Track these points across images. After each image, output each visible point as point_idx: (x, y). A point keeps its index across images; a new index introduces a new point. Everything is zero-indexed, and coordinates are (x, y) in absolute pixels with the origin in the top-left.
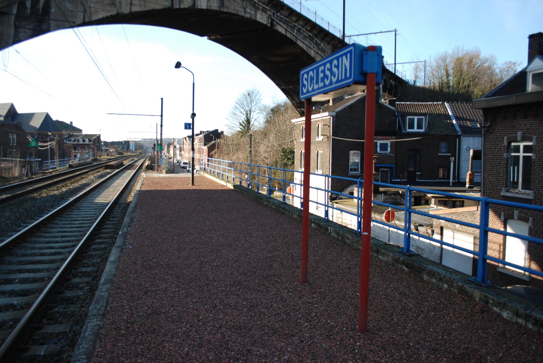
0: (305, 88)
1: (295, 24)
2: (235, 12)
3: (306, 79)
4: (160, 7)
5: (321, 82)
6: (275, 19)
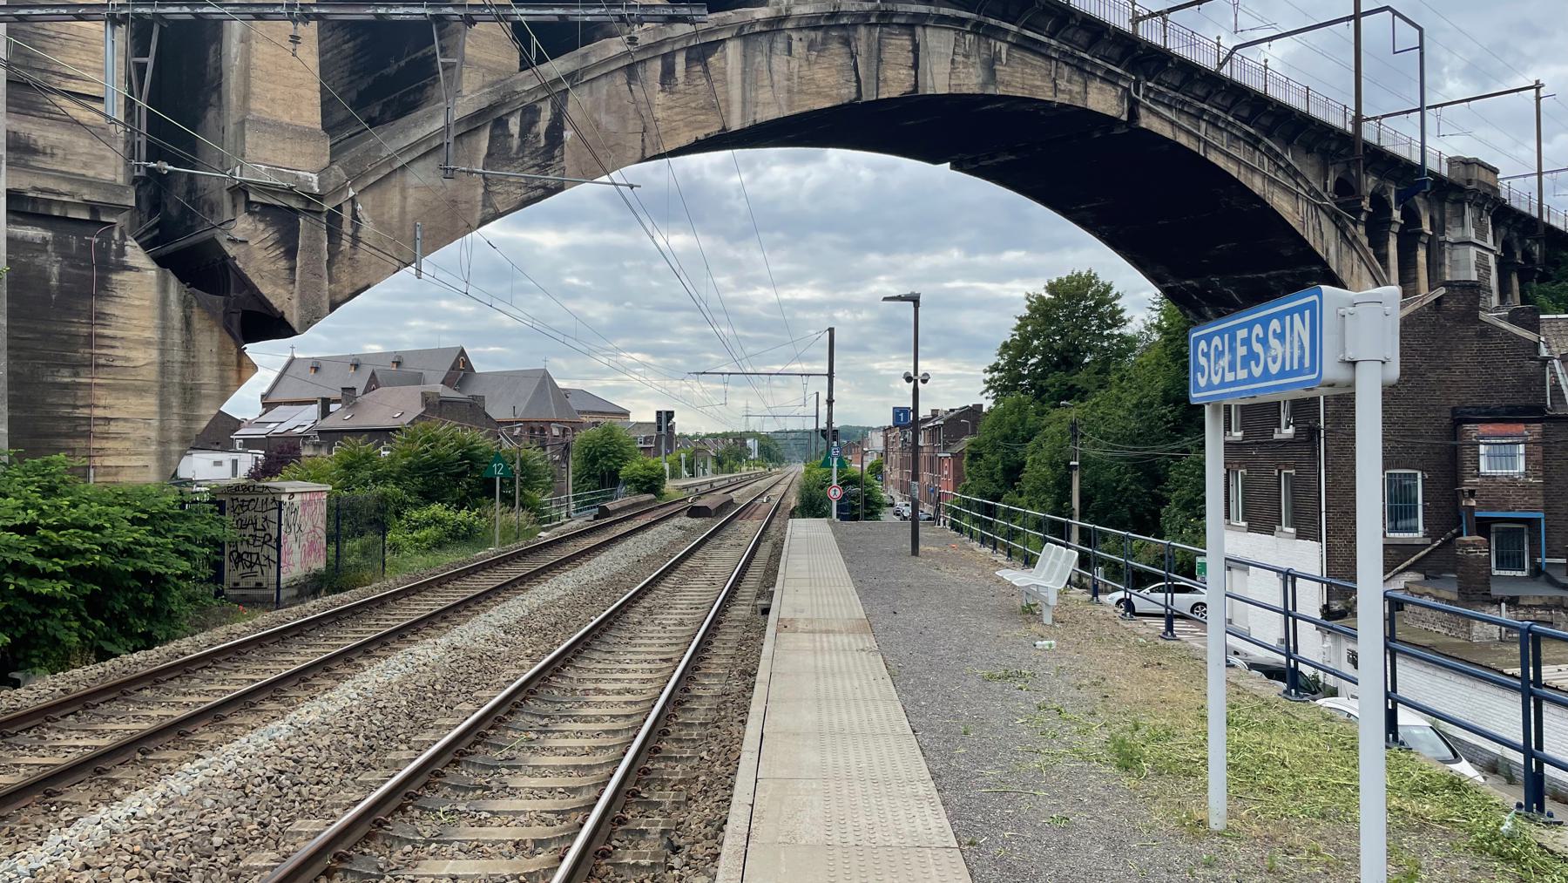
0: (1203, 376)
1: (1202, 105)
2: (1026, 94)
3: (1204, 354)
4: (827, 104)
5: (1242, 368)
6: (1141, 98)
